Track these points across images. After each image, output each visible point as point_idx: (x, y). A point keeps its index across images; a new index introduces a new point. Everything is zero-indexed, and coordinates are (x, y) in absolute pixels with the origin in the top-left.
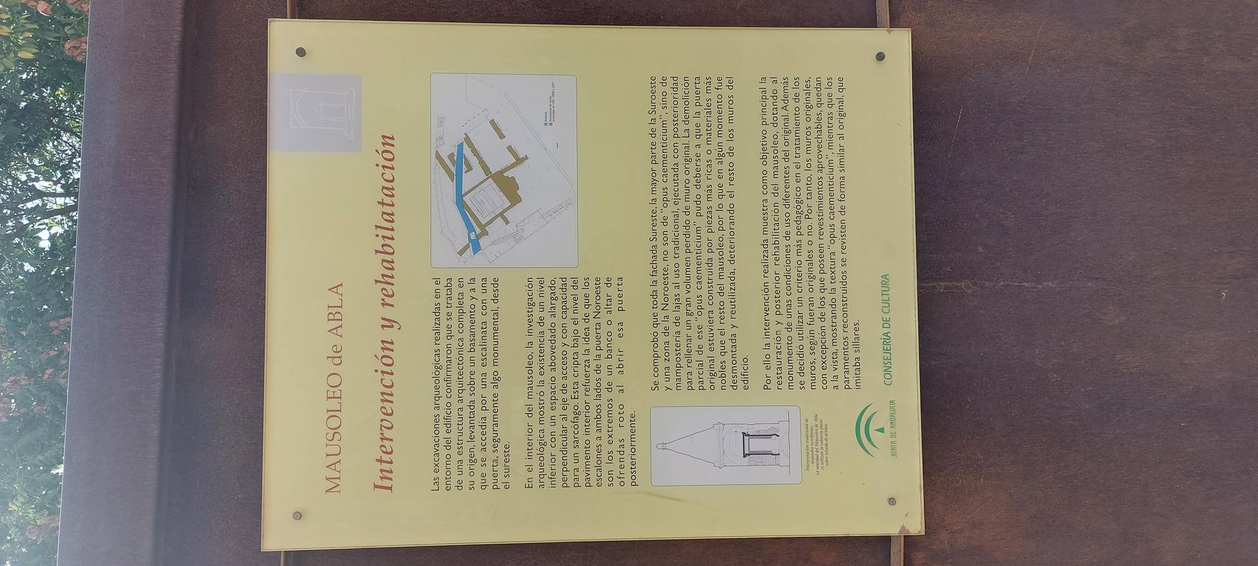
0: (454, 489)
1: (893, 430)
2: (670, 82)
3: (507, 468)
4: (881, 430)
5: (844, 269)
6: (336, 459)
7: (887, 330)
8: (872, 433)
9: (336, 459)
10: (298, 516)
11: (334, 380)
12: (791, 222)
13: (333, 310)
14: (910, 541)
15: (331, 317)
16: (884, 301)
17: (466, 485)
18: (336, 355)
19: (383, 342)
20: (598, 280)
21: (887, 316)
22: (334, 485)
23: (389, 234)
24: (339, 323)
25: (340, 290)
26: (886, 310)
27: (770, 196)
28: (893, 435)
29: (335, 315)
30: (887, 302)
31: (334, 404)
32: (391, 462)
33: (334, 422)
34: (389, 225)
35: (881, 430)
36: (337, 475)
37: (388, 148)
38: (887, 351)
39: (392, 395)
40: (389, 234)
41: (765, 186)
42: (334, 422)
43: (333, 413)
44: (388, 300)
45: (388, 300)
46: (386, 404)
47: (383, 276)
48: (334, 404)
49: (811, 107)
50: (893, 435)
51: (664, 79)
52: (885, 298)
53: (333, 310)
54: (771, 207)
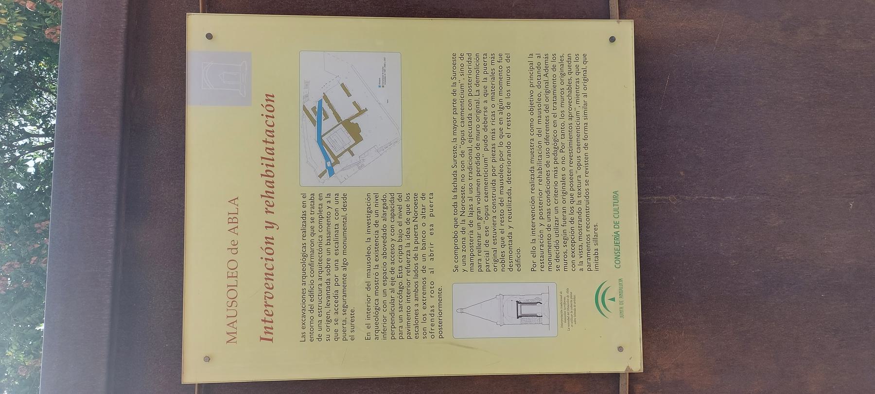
0: (316, 340)
1: (621, 300)
2: (466, 57)
3: (353, 326)
4: (613, 299)
5: (587, 187)
6: (233, 319)
7: (617, 230)
8: (606, 301)
9: (233, 319)
10: (207, 359)
11: (233, 265)
12: (551, 154)
13: (232, 216)
14: (633, 377)
15: (230, 220)
16: (615, 210)
17: (324, 337)
18: (234, 247)
19: (266, 238)
20: (416, 195)
21: (617, 220)
22: (232, 337)
23: (270, 163)
24: (236, 225)
25: (237, 202)
26: (616, 216)
27: (535, 137)
28: (621, 303)
29: (233, 219)
30: (617, 210)
31: (232, 281)
32: (272, 322)
33: (232, 294)
34: (270, 157)
35: (613, 299)
36: (234, 331)
37: (270, 103)
38: (617, 244)
39: (272, 275)
40: (270, 163)
41: (532, 130)
42: (232, 294)
43: (231, 288)
44: (270, 209)
45: (270, 209)
46: (268, 281)
47: (267, 192)
48: (232, 281)
49: (564, 75)
50: (621, 303)
51: (462, 55)
52: (616, 207)
53: (232, 216)
54: (536, 144)
